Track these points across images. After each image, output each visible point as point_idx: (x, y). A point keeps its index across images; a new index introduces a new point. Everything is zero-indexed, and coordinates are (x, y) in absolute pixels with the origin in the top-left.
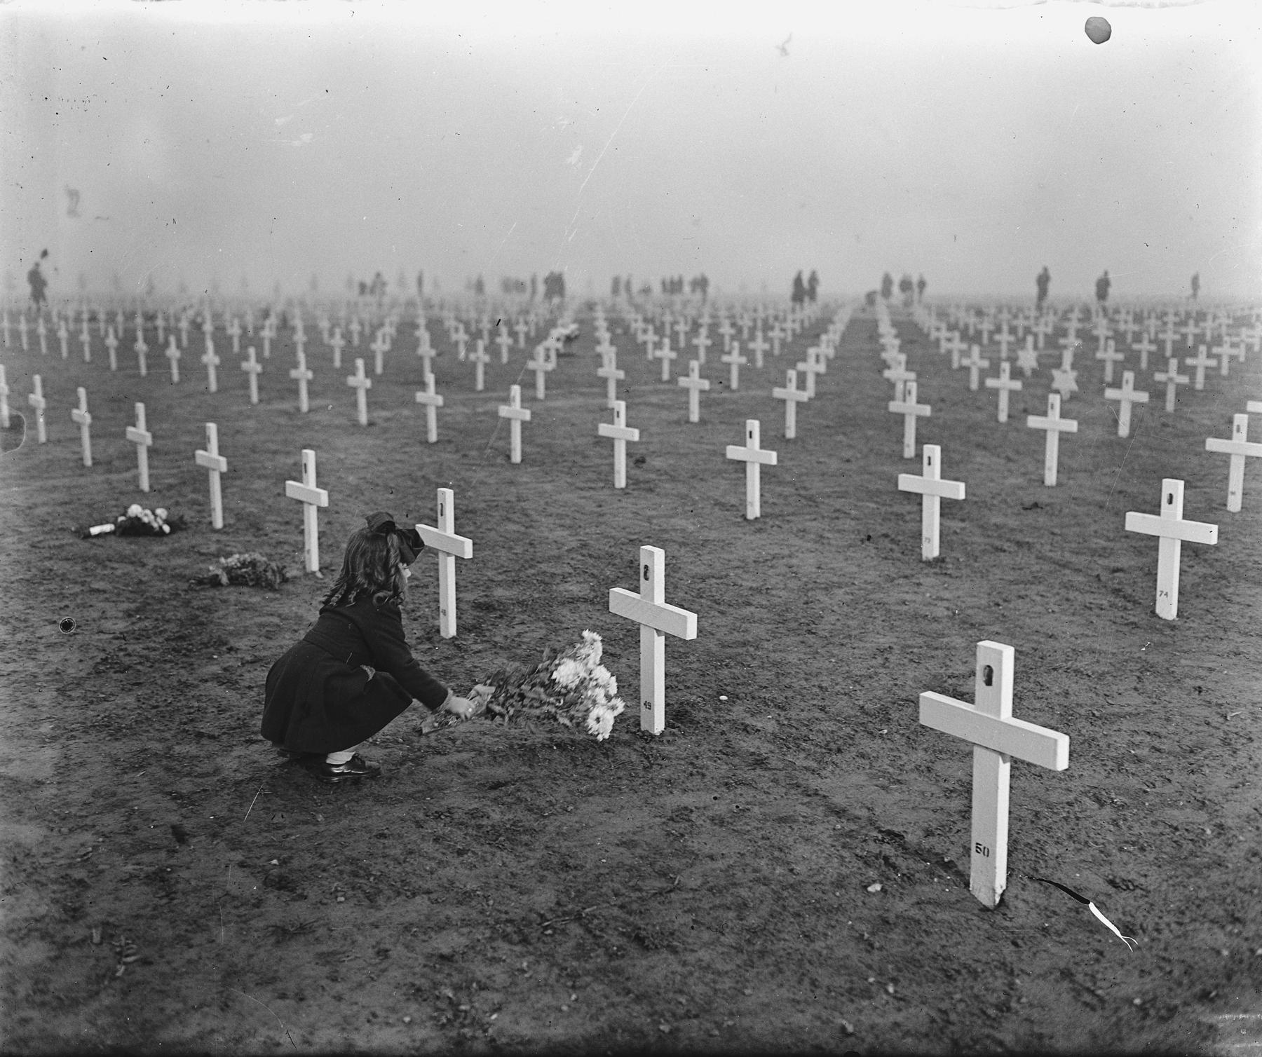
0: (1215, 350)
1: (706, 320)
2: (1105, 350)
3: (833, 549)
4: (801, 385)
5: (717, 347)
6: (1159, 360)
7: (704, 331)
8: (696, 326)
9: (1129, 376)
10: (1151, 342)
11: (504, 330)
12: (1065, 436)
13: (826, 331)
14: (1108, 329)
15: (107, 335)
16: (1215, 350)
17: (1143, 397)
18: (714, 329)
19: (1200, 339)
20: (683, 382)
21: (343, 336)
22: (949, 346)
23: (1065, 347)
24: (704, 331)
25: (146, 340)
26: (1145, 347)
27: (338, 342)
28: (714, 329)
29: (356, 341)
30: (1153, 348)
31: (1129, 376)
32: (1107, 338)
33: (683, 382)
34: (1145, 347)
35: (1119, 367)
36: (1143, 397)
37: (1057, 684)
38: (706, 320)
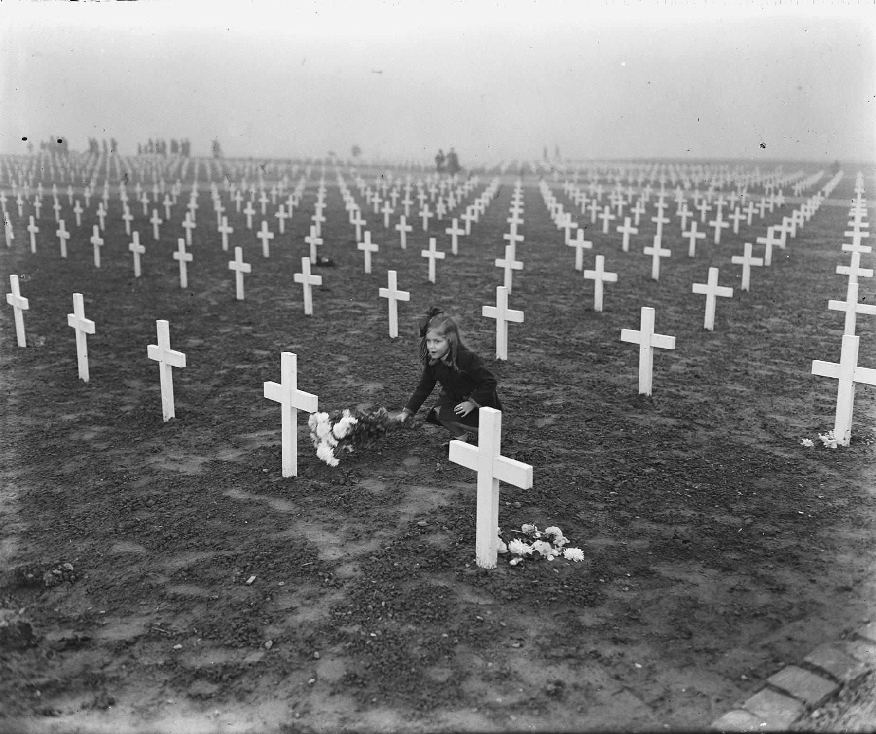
0: (745, 210)
1: (408, 189)
2: (682, 210)
3: (48, 576)
4: (286, 211)
5: (416, 207)
6: (712, 215)
7: (407, 196)
8: (402, 194)
9: (694, 225)
10: (708, 205)
11: (264, 194)
12: (704, 281)
13: (484, 191)
14: (684, 197)
15: (74, 205)
16: (745, 210)
17: (702, 235)
18: (414, 196)
19: (737, 203)
20: (398, 227)
21: (253, 207)
22: (580, 200)
23: (507, 242)
24: (407, 196)
25: (60, 204)
26: (704, 208)
27: (249, 211)
28: (414, 196)
29: (264, 210)
30: (709, 208)
31: (694, 225)
32: (683, 203)
33: (398, 227)
34: (704, 208)
35: (689, 220)
36: (702, 235)
37: (521, 439)
38: (408, 189)
